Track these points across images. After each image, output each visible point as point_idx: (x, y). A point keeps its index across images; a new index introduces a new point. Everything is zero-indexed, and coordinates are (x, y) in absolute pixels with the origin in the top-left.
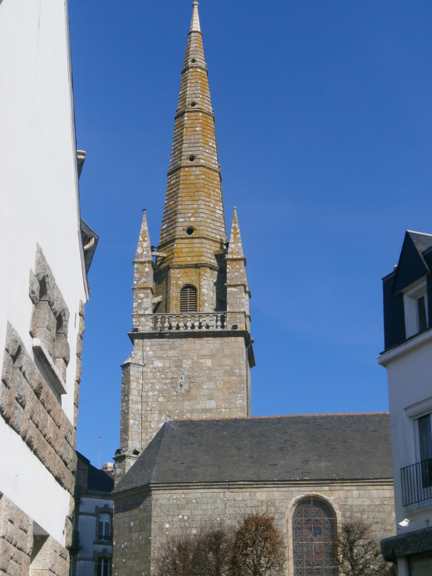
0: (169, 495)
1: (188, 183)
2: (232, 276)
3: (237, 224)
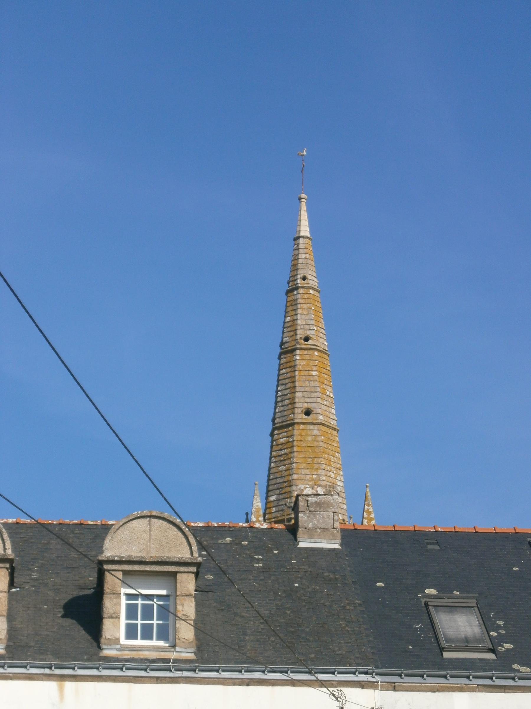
1: (304, 445)
3: (370, 507)
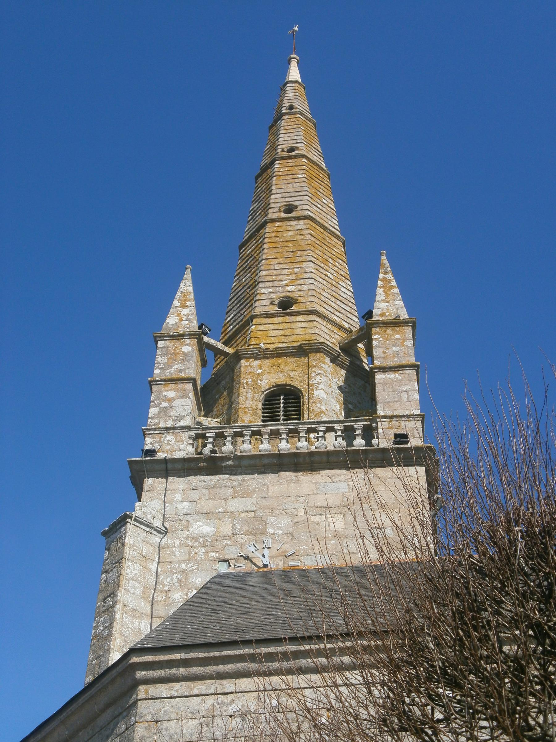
0: (210, 700)
2: (385, 353)
